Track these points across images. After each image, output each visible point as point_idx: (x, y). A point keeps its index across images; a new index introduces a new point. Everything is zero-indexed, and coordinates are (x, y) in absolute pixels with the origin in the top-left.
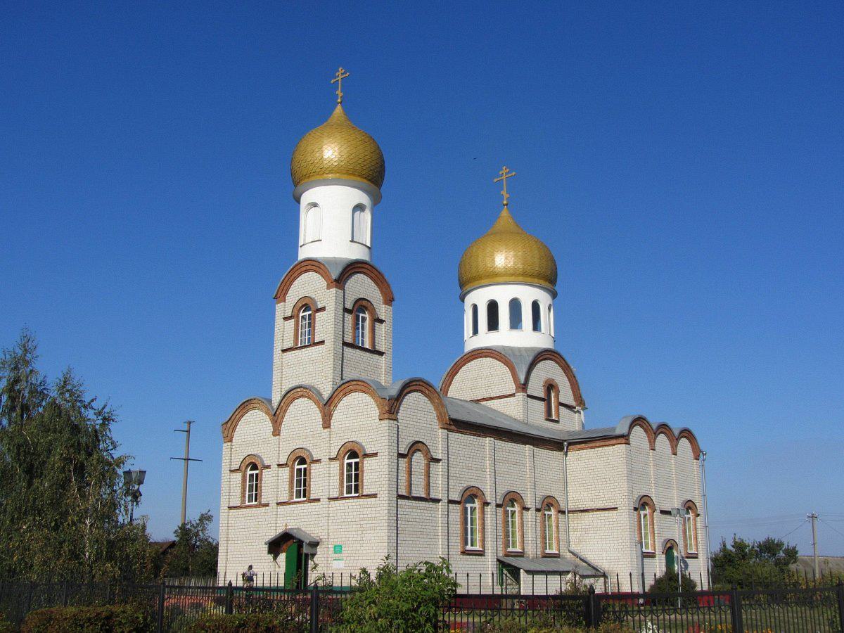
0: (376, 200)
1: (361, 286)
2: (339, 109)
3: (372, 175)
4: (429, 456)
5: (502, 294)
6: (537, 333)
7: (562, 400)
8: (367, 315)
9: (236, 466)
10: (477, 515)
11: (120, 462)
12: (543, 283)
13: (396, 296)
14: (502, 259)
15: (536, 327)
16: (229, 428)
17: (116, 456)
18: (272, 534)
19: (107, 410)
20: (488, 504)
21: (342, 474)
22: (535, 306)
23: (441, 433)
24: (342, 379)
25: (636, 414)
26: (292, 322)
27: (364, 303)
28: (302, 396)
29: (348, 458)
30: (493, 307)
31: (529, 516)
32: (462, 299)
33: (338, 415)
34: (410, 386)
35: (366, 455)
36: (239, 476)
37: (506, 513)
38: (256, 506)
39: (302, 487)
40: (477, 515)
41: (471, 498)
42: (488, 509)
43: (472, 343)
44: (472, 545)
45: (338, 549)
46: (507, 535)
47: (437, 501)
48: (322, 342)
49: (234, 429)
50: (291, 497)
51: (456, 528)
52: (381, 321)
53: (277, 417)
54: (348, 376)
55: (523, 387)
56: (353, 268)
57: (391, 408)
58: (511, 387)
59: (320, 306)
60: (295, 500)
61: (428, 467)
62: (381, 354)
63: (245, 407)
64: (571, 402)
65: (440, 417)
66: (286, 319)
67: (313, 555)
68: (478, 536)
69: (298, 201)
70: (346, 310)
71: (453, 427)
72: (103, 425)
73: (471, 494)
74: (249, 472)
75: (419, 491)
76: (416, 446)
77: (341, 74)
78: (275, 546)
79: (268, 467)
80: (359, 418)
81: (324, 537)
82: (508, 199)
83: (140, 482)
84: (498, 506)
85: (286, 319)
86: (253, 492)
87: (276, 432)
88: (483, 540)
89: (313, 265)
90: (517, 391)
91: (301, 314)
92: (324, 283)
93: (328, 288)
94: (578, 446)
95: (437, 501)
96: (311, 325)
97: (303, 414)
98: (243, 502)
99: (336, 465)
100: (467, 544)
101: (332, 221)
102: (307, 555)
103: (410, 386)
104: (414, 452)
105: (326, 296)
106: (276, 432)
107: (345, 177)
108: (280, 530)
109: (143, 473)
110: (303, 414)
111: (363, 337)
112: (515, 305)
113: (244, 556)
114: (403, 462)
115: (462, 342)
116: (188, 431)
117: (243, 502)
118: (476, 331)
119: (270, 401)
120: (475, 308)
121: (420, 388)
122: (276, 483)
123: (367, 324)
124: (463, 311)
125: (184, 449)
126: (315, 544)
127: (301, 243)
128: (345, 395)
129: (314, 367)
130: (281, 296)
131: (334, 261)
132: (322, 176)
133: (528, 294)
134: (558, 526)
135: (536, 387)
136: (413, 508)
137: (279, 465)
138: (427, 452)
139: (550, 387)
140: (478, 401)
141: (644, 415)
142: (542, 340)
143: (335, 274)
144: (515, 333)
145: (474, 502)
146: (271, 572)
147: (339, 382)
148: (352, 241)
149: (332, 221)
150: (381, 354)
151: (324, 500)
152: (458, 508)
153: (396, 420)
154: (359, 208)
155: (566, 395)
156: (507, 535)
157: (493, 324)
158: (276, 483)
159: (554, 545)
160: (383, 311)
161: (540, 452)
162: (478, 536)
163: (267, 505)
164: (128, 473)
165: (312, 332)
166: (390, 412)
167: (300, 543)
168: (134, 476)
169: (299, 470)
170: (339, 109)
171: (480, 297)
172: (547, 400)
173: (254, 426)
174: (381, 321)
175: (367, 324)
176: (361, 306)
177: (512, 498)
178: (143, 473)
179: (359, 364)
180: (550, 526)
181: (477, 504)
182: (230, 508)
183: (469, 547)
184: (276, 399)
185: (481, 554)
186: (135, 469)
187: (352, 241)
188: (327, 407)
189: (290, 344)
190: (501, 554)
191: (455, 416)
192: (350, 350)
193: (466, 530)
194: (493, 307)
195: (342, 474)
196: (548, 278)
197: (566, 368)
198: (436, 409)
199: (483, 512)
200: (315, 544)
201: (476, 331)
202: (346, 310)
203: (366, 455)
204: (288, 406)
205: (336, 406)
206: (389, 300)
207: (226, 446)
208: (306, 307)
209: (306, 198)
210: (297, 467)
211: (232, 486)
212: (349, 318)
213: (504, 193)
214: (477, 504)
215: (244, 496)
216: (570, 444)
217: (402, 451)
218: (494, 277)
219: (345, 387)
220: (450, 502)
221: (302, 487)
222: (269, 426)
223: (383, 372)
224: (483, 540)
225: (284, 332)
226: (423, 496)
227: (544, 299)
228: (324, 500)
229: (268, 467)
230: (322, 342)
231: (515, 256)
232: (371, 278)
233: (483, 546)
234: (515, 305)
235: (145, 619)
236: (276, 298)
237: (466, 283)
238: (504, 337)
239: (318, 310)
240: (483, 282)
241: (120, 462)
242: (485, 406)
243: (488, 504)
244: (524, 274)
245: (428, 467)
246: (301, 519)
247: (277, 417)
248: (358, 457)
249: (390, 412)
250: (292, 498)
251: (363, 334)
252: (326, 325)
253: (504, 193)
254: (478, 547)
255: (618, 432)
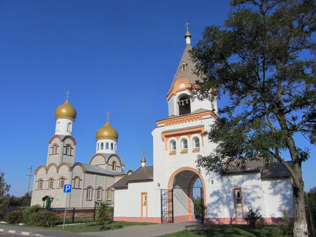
0: (74, 121)
1: (68, 141)
2: (67, 101)
3: (73, 117)
4: (80, 179)
5: (105, 141)
6: (112, 150)
7: (117, 165)
8: (69, 148)
9: (37, 181)
10: (91, 192)
11: (5, 184)
12: (114, 139)
13: (77, 143)
14: (106, 133)
15: (112, 149)
16: (36, 171)
17: (4, 182)
18: (43, 196)
19: (3, 172)
20: (93, 189)
21: (60, 183)
22: (112, 144)
23: (83, 174)
24: (62, 162)
25: (130, 170)
26: (52, 149)
27: (69, 145)
28: (53, 165)
29: (62, 179)
30: (102, 144)
31: (104, 192)
32: (96, 141)
33: (60, 170)
34: (76, 164)
35: (65, 179)
36: (37, 183)
37: (98, 191)
38: (41, 190)
39: (51, 186)
40: (91, 192)
41: (90, 188)
42: (93, 190)
43: (98, 152)
44: (89, 198)
45: (58, 200)
46: (98, 196)
47: (81, 189)
48: (58, 154)
49: (37, 172)
50: (49, 188)
51: (85, 195)
52: (73, 149)
53: (47, 170)
54: (64, 161)
55: (107, 163)
56: (67, 137)
57: (71, 169)
58: (105, 163)
59: (58, 146)
60: (50, 188)
61: (79, 181)
62: (72, 156)
63: (40, 167)
64: (119, 166)
65: (83, 171)
66: (51, 148)
67: (52, 201)
68: (91, 196)
69: (56, 121)
70: (64, 147)
71: (86, 173)
72: (2, 176)
73: (89, 187)
74: (40, 182)
75: (77, 187)
76: (76, 177)
77: (68, 92)
78: (44, 199)
79: (44, 181)
80: (64, 171)
81: (55, 197)
82: (109, 119)
83: (9, 187)
84: (96, 190)
85: (51, 148)
86: (41, 186)
87: (47, 173)
88: (92, 197)
89: (57, 136)
90: (106, 163)
91: (54, 147)
92: (60, 141)
93: (60, 142)
94: (117, 176)
95: (81, 189)
96: (56, 149)
97: (53, 169)
98: (38, 189)
99: (59, 181)
100: (88, 198)
101: (63, 127)
102: (51, 201)
103: (76, 164)
104: (76, 178)
105: (60, 144)
106: (47, 173)
107: (66, 117)
108: (46, 195)
109: (10, 185)
110: (53, 169)
111: (68, 152)
112: (107, 144)
113: (37, 201)
114: (73, 181)
115: (95, 151)
116: (31, 169)
117: (38, 189)
118: (98, 149)
119: (46, 166)
120: (98, 144)
121: (79, 164)
122: (46, 185)
123: (69, 149)
124: (96, 145)
125: (30, 173)
126: (53, 199)
127: (56, 131)
128: (62, 166)
129: (55, 159)
130: (50, 142)
131: (62, 136)
132: (62, 116)
133: (110, 141)
134: (111, 194)
135: (110, 162)
136: (75, 190)
137: (47, 181)
138: (79, 178)
139: (114, 162)
140: (97, 165)
141: (132, 170)
142: (113, 152)
143: (62, 139)
144: (107, 150)
145: (90, 189)
146: (42, 204)
147: (61, 162)
148: (67, 131)
149: (63, 127)
150: (72, 156)
151: (56, 189)
152: (86, 190)
153: (72, 171)
154: (70, 123)
155: (118, 164)
156: (98, 196)
157: (102, 148)
158: (46, 185)
159: (110, 198)
160: (73, 146)
161: (108, 177)
162: (91, 196)
163: (43, 189)
164: (7, 185)
165: (56, 151)
166: (71, 170)
167: (49, 198)
168: (8, 186)
169: (51, 182)
170: (67, 101)
171: (100, 142)
172: (113, 165)
173: (42, 171)
174: (73, 149)
175: (69, 149)
176: (68, 145)
177: (99, 188)
178: (10, 185)
179: (67, 159)
180: (109, 194)
181: (91, 189)
182: (35, 190)
183: (88, 199)
184: (47, 166)
185: (91, 200)
186: (9, 184)
187: (67, 131)
188: (58, 168)
189: (51, 153)
190: (96, 200)
191: (87, 170)
192: (65, 155)
193: (88, 195)
194: (102, 144)
195: (60, 183)
196: (116, 138)
197: (118, 158)
198: (82, 169)
199: (92, 191)
200: (53, 199)
201: (98, 149)
202: (64, 147)
203: (65, 179)
204: (50, 167)
205: (60, 168)
206: (75, 144)
207: (35, 176)
208: (56, 146)
209: (58, 120)
210: (51, 181)
211: (35, 185)
212: (65, 148)
213: (108, 117)
214: (91, 189)
215: (38, 187)
216: (115, 176)
217: (73, 178)
218: (103, 137)
219: (62, 164)
220: (84, 189)
221: (51, 186)
222: (45, 172)
223: (72, 161)
224: (92, 197)
225: (50, 151)
226: (78, 188)
227: (114, 142)
228: (56, 189)
229: (44, 181)
230: (58, 154)
231: (108, 133)
232: (71, 139)
233: (92, 198)
234: (107, 144)
235: (2, 213)
236: (49, 143)
237: (98, 138)
238: (105, 151)
239: (58, 146)
240: (101, 138)
241: (5, 184)
242: (99, 167)
243: (93, 189)
244: (110, 137)
245: (79, 181)
246: (50, 193)
247: (47, 170)
248: (63, 179)
249: (71, 170)
250: (49, 188)
251: (68, 152)
252: (59, 150)
253: (108, 117)
254: (90, 199)
255: (125, 174)
